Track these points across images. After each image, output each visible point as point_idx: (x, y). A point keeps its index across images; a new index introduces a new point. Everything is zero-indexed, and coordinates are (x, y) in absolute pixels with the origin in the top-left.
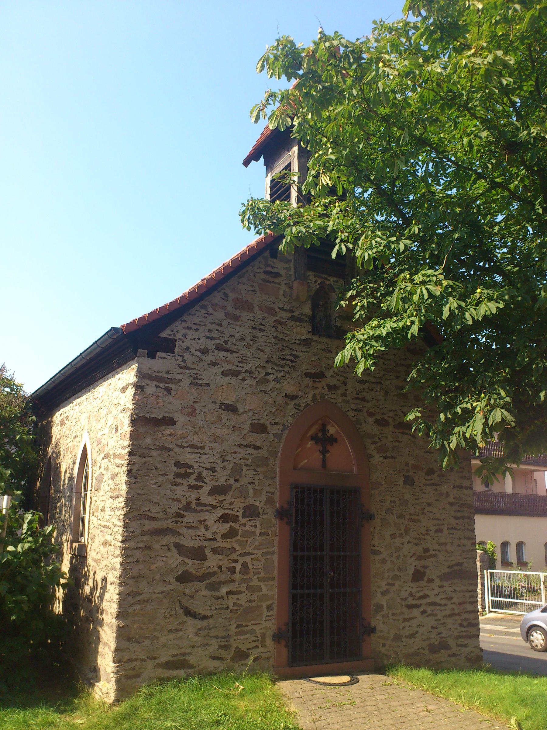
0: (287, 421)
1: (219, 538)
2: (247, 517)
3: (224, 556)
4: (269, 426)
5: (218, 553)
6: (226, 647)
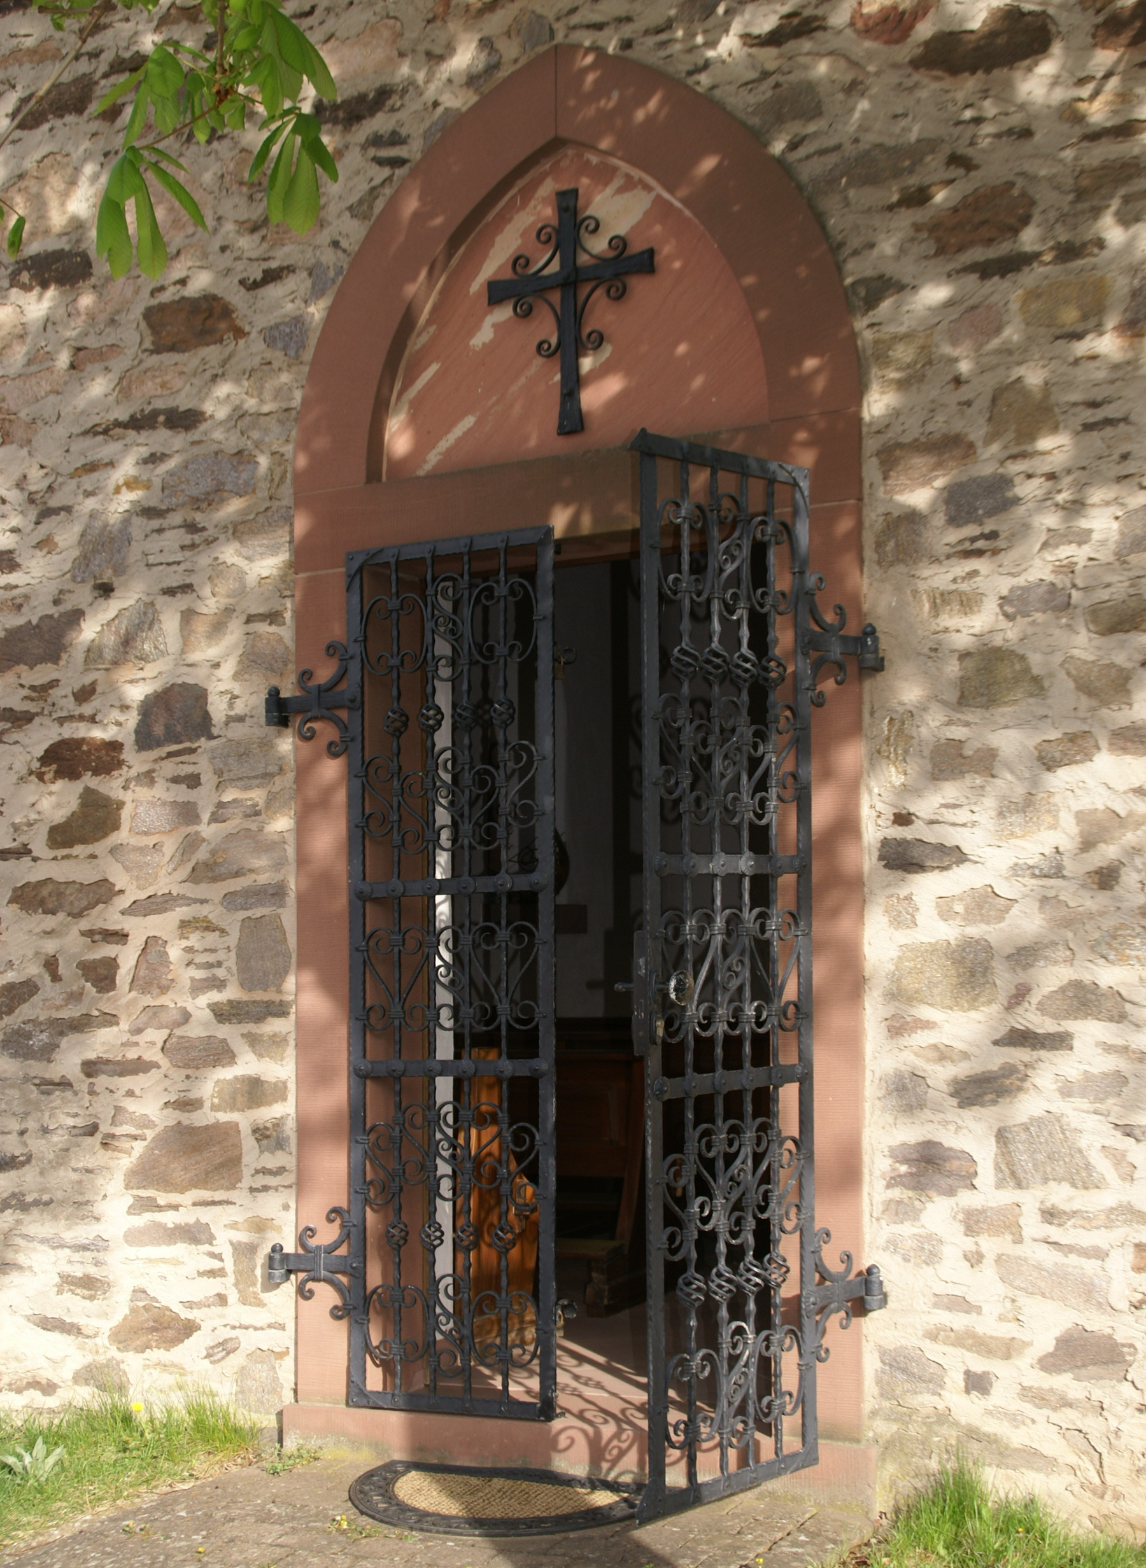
0: (336, 244)
1: (39, 847)
2: (159, 744)
3: (61, 916)
4: (237, 298)
5: (42, 903)
6: (90, 1285)
